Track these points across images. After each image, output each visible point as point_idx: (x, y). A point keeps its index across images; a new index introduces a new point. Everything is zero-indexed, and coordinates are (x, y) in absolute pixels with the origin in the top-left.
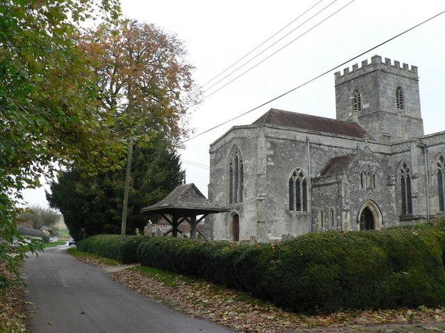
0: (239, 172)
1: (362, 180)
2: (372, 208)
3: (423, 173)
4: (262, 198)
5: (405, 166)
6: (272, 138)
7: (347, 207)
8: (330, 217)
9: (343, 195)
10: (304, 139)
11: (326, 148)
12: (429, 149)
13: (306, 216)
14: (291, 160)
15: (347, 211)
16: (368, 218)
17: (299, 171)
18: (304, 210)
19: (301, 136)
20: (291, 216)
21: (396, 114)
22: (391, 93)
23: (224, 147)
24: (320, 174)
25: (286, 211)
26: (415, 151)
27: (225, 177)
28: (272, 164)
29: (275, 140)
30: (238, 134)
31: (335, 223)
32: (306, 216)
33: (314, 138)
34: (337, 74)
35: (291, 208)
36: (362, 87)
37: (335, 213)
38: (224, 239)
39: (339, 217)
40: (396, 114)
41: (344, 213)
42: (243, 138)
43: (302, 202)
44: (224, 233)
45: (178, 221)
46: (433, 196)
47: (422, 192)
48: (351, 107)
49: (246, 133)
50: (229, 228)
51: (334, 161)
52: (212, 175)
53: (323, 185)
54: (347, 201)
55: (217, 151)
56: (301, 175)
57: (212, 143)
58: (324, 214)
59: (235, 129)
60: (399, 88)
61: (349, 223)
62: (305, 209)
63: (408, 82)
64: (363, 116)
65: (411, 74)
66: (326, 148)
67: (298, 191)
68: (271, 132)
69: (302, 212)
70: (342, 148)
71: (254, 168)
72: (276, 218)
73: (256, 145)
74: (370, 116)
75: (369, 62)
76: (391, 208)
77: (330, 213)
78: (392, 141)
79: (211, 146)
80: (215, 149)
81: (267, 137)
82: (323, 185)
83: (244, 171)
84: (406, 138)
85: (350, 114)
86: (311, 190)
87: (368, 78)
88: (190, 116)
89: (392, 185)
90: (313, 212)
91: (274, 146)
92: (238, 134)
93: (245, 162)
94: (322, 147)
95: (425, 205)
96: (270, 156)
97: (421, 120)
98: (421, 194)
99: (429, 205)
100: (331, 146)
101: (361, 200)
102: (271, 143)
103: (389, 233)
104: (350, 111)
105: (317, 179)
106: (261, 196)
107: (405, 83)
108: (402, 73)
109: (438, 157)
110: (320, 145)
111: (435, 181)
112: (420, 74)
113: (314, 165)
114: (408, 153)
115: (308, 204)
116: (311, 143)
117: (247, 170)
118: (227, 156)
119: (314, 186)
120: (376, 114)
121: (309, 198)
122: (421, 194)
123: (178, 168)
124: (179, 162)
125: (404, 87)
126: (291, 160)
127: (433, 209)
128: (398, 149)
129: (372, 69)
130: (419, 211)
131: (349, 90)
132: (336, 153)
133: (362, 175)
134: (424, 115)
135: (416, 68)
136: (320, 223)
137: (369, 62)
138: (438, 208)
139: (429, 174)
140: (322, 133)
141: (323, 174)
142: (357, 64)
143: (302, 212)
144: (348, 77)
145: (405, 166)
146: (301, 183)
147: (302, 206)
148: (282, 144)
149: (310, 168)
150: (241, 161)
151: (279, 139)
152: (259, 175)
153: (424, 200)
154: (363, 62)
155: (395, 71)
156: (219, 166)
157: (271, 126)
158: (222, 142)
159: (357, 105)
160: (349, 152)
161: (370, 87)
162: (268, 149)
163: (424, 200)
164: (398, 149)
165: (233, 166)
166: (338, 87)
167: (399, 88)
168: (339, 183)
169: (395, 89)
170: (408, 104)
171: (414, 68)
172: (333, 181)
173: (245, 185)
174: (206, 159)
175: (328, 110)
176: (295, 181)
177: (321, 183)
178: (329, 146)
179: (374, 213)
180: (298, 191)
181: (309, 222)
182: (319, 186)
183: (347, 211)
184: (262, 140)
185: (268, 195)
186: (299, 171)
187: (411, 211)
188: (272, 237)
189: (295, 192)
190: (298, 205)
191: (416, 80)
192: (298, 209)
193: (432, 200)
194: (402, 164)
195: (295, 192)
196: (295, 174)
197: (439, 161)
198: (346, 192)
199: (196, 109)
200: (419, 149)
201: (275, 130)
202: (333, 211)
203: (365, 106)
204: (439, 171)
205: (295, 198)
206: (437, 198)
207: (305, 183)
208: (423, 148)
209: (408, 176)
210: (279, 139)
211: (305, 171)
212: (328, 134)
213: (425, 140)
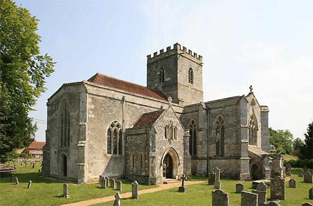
0: (67, 122)
1: (165, 132)
2: (171, 154)
11: (138, 107)
12: (212, 111)
14: (109, 114)
17: (117, 123)
21: (188, 87)
24: (133, 126)
27: (58, 124)
28: (93, 116)
29: (96, 97)
31: (143, 166)
32: (121, 158)
34: (149, 56)
36: (166, 65)
37: (143, 157)
38: (57, 174)
39: (147, 161)
40: (188, 87)
44: (57, 169)
46: (212, 144)
47: (205, 141)
48: (157, 80)
50: (61, 166)
52: (49, 123)
58: (135, 158)
59: (65, 86)
60: (191, 69)
63: (197, 66)
64: (166, 86)
65: (198, 59)
69: (118, 155)
70: (150, 107)
72: (96, 161)
75: (172, 48)
79: (48, 100)
83: (71, 121)
85: (156, 85)
89: (187, 137)
93: (72, 114)
95: (206, 150)
97: (203, 93)
98: (204, 143)
99: (208, 150)
100: (143, 105)
101: (164, 148)
103: (251, 166)
106: (82, 143)
107: (195, 67)
108: (193, 59)
111: (214, 133)
112: (204, 60)
114: (196, 113)
116: (126, 101)
118: (59, 109)
122: (204, 143)
126: (109, 114)
127: (211, 153)
129: (173, 53)
130: (202, 154)
131: (157, 68)
134: (205, 89)
136: (132, 164)
140: (136, 95)
142: (163, 49)
143: (118, 155)
145: (193, 122)
147: (118, 151)
151: (99, 96)
153: (206, 146)
154: (167, 48)
155: (187, 56)
156: (54, 116)
161: (171, 66)
165: (64, 116)
166: (149, 65)
167: (191, 69)
173: (71, 133)
174: (45, 109)
178: (140, 105)
181: (123, 163)
186: (117, 123)
188: (156, 172)
196: (112, 126)
203: (167, 79)
210: (99, 96)
213: (209, 105)
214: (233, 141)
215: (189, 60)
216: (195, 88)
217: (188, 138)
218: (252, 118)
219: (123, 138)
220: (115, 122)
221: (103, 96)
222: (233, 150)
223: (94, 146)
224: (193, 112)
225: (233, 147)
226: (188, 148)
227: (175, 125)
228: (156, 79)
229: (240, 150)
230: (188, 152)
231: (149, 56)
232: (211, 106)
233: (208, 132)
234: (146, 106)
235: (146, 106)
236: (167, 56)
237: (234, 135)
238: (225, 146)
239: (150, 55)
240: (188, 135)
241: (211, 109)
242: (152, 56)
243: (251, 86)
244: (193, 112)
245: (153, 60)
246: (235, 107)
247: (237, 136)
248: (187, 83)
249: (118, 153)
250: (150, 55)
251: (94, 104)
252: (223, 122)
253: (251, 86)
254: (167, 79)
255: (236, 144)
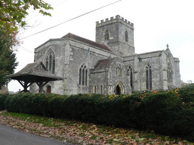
2: (120, 86)
3: (139, 71)
4: (67, 77)
5: (130, 67)
6: (72, 46)
7: (111, 84)
8: (100, 89)
9: (109, 78)
10: (87, 49)
11: (97, 55)
12: (142, 60)
13: (86, 88)
14: (81, 59)
15: (111, 86)
16: (118, 90)
17: (84, 65)
18: (83, 85)
19: (86, 47)
20: (80, 87)
21: (125, 44)
22: (123, 33)
23: (44, 50)
24: (93, 68)
25: (78, 85)
26: (137, 60)
28: (72, 59)
29: (74, 47)
30: (53, 43)
33: (92, 49)
34: (97, 22)
35: (80, 84)
37: (103, 87)
39: (105, 89)
40: (125, 44)
41: (109, 87)
42: (55, 45)
43: (85, 81)
45: (28, 85)
46: (143, 82)
48: (104, 39)
49: (58, 42)
51: (100, 61)
53: (97, 73)
54: (111, 81)
55: (38, 52)
56: (85, 67)
57: (36, 48)
58: (96, 88)
59: (51, 40)
60: (126, 32)
61: (111, 91)
62: (86, 85)
64: (110, 43)
66: (97, 55)
67: (83, 75)
68: (72, 43)
70: (104, 56)
71: (62, 62)
72: (73, 88)
73: (64, 49)
74: (114, 43)
75: (114, 18)
76: (128, 86)
77: (100, 87)
78: (124, 56)
79: (35, 49)
80: (38, 51)
81: (70, 45)
82: (97, 73)
84: (128, 55)
85: (103, 42)
86: (89, 75)
87: (114, 25)
88: (20, 35)
90: (90, 86)
91: (73, 50)
92: (53, 43)
94: (95, 54)
95: (140, 86)
96: (71, 55)
97: (134, 48)
98: (138, 81)
101: (116, 81)
102: (72, 48)
104: (103, 40)
105: (93, 70)
106: (66, 76)
107: (129, 30)
108: (128, 25)
109: (147, 64)
110: (94, 53)
112: (135, 26)
113: (91, 63)
114: (132, 61)
115: (88, 82)
117: (58, 63)
119: (91, 73)
120: (116, 42)
121: (88, 79)
123: (14, 60)
124: (15, 57)
125: (128, 32)
126: (81, 59)
127: (143, 88)
128: (127, 59)
129: (116, 21)
131: (103, 30)
132: (101, 57)
133: (117, 69)
135: (133, 24)
137: (114, 18)
138: (146, 88)
139: (142, 72)
140: (96, 47)
141: (95, 67)
144: (103, 24)
145: (130, 67)
146: (85, 71)
148: (77, 50)
149: (89, 64)
150: (54, 57)
152: (65, 65)
153: (139, 84)
157: (72, 40)
158: (42, 47)
159: (107, 37)
160: (107, 58)
161: (114, 29)
162: (71, 52)
163: (139, 84)
164: (127, 59)
165: (49, 61)
166: (97, 28)
167: (126, 32)
168: (107, 72)
169: (125, 32)
170: (129, 40)
171: (132, 24)
172: (103, 70)
175: (92, 37)
176: (82, 69)
177: (96, 72)
178: (98, 54)
179: (121, 88)
180: (83, 75)
182: (95, 73)
183: (111, 86)
184: (68, 46)
185: (69, 76)
186: (84, 65)
187: (151, 87)
189: (82, 75)
190: (83, 82)
191: (133, 29)
192: (83, 84)
193: (143, 84)
194: (128, 66)
195: (82, 75)
196: (82, 66)
197: (147, 66)
198: (110, 76)
199: (23, 32)
200: (138, 60)
201: (74, 42)
202: (102, 86)
203: (111, 38)
204: (147, 70)
205: (82, 78)
206: (145, 83)
207: (87, 71)
208: (140, 59)
209: (150, 70)
211: (87, 65)
212: (98, 48)
213: (141, 56)
214: (158, 79)
215: (125, 26)
216: (130, 45)
217: (130, 76)
218: (169, 65)
219: (88, 75)
220: (84, 64)
221: (78, 47)
222: (158, 85)
223: (72, 79)
224: (130, 61)
225: (158, 84)
226: (130, 82)
227: (122, 66)
228: (102, 37)
229: (163, 85)
230: (130, 85)
231: (97, 22)
232: (142, 57)
233: (140, 74)
234: (101, 55)
235: (101, 55)
236: (111, 23)
237: (158, 76)
238: (153, 83)
239: (103, 20)
240: (130, 74)
241: (143, 59)
242: (100, 22)
243: (168, 45)
244: (130, 61)
245: (100, 25)
246: (158, 57)
247: (160, 76)
248: (124, 41)
249: (85, 85)
250: (103, 20)
251: (73, 52)
252: (150, 67)
253: (168, 45)
254: (111, 38)
255: (160, 81)
